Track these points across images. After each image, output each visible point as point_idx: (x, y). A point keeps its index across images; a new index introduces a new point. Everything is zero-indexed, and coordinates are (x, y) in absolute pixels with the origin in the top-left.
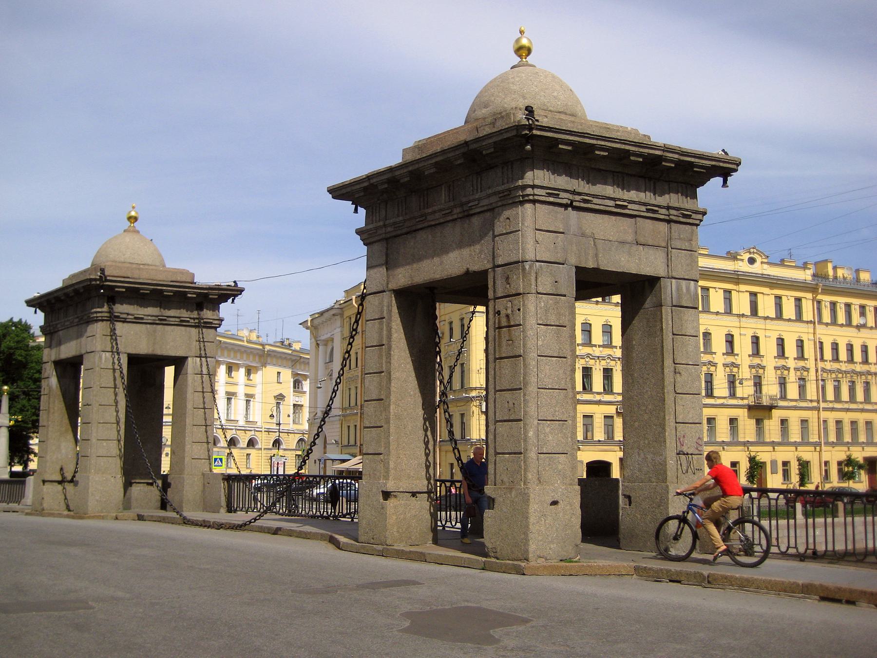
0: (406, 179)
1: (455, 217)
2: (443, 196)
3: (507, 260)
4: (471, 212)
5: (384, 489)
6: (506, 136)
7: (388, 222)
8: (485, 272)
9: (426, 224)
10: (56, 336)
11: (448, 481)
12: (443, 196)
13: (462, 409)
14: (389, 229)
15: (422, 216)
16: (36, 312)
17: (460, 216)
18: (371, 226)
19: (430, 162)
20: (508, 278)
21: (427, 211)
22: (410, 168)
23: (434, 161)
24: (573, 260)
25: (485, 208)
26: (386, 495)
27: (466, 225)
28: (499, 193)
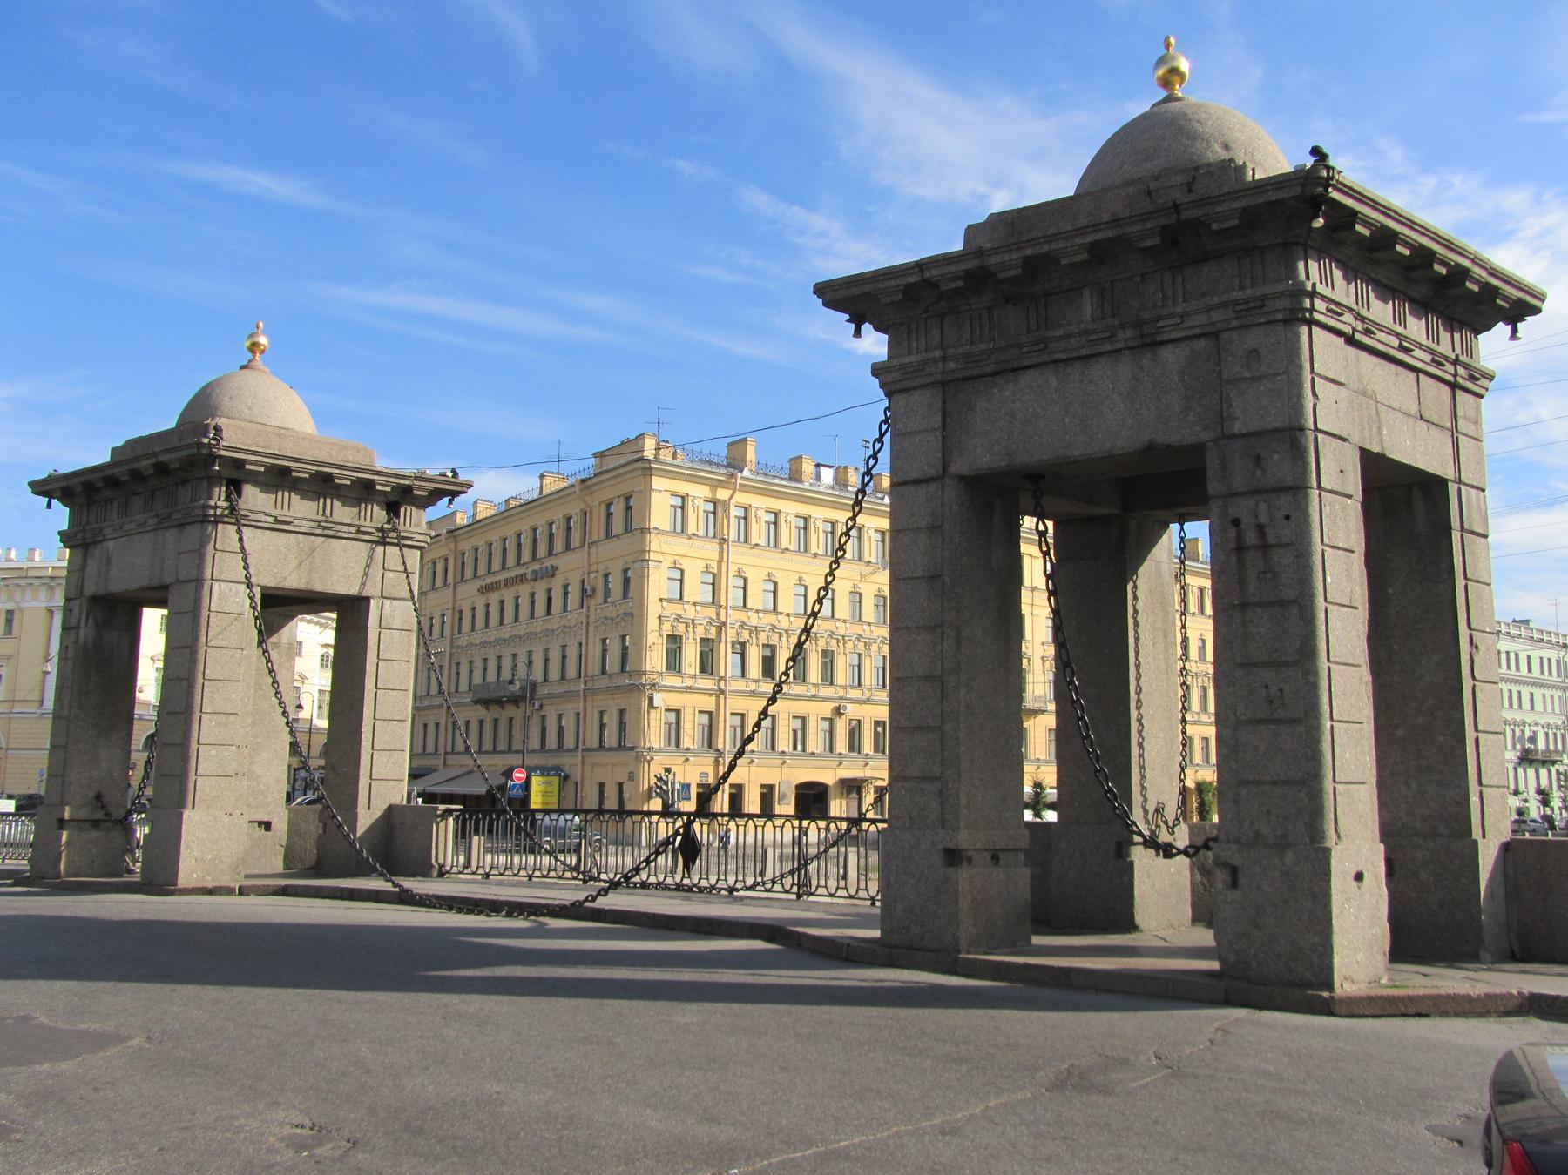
0: (1012, 273)
1: (1120, 345)
2: (1087, 306)
3: (1254, 425)
4: (1159, 338)
5: (951, 845)
6: (1273, 196)
7: (950, 352)
8: (1199, 449)
9: (1046, 358)
10: (97, 551)
11: (841, 819)
12: (1087, 306)
13: (622, 701)
14: (952, 365)
15: (1037, 342)
16: (49, 506)
17: (1132, 343)
18: (894, 362)
19: (1078, 241)
20: (1258, 458)
21: (1050, 334)
22: (1029, 252)
23: (1089, 239)
24: (1356, 438)
25: (1197, 331)
26: (953, 857)
27: (1146, 363)
28: (1236, 302)
